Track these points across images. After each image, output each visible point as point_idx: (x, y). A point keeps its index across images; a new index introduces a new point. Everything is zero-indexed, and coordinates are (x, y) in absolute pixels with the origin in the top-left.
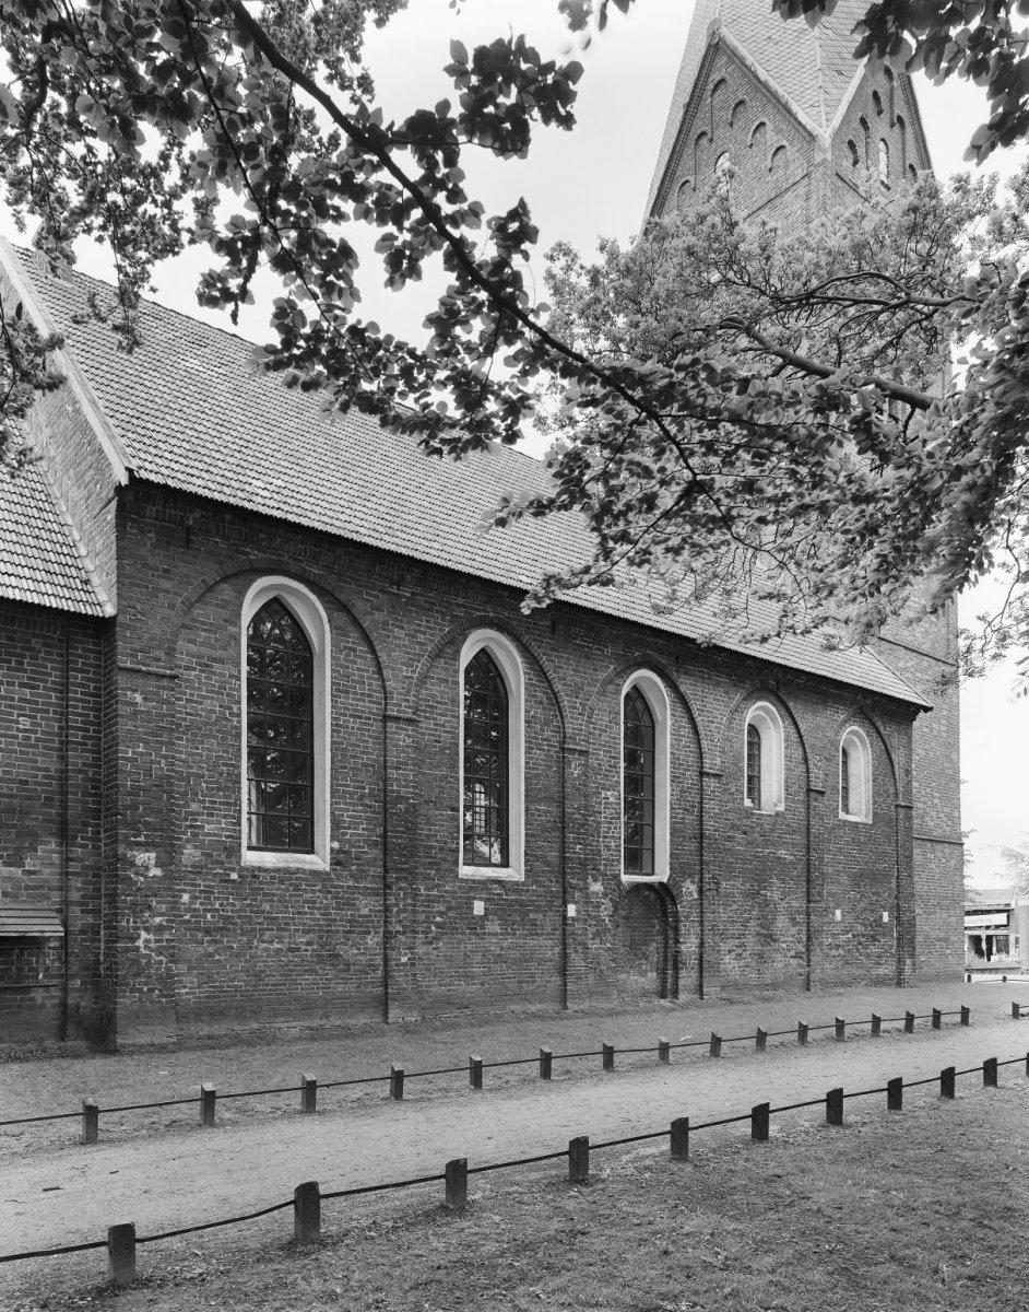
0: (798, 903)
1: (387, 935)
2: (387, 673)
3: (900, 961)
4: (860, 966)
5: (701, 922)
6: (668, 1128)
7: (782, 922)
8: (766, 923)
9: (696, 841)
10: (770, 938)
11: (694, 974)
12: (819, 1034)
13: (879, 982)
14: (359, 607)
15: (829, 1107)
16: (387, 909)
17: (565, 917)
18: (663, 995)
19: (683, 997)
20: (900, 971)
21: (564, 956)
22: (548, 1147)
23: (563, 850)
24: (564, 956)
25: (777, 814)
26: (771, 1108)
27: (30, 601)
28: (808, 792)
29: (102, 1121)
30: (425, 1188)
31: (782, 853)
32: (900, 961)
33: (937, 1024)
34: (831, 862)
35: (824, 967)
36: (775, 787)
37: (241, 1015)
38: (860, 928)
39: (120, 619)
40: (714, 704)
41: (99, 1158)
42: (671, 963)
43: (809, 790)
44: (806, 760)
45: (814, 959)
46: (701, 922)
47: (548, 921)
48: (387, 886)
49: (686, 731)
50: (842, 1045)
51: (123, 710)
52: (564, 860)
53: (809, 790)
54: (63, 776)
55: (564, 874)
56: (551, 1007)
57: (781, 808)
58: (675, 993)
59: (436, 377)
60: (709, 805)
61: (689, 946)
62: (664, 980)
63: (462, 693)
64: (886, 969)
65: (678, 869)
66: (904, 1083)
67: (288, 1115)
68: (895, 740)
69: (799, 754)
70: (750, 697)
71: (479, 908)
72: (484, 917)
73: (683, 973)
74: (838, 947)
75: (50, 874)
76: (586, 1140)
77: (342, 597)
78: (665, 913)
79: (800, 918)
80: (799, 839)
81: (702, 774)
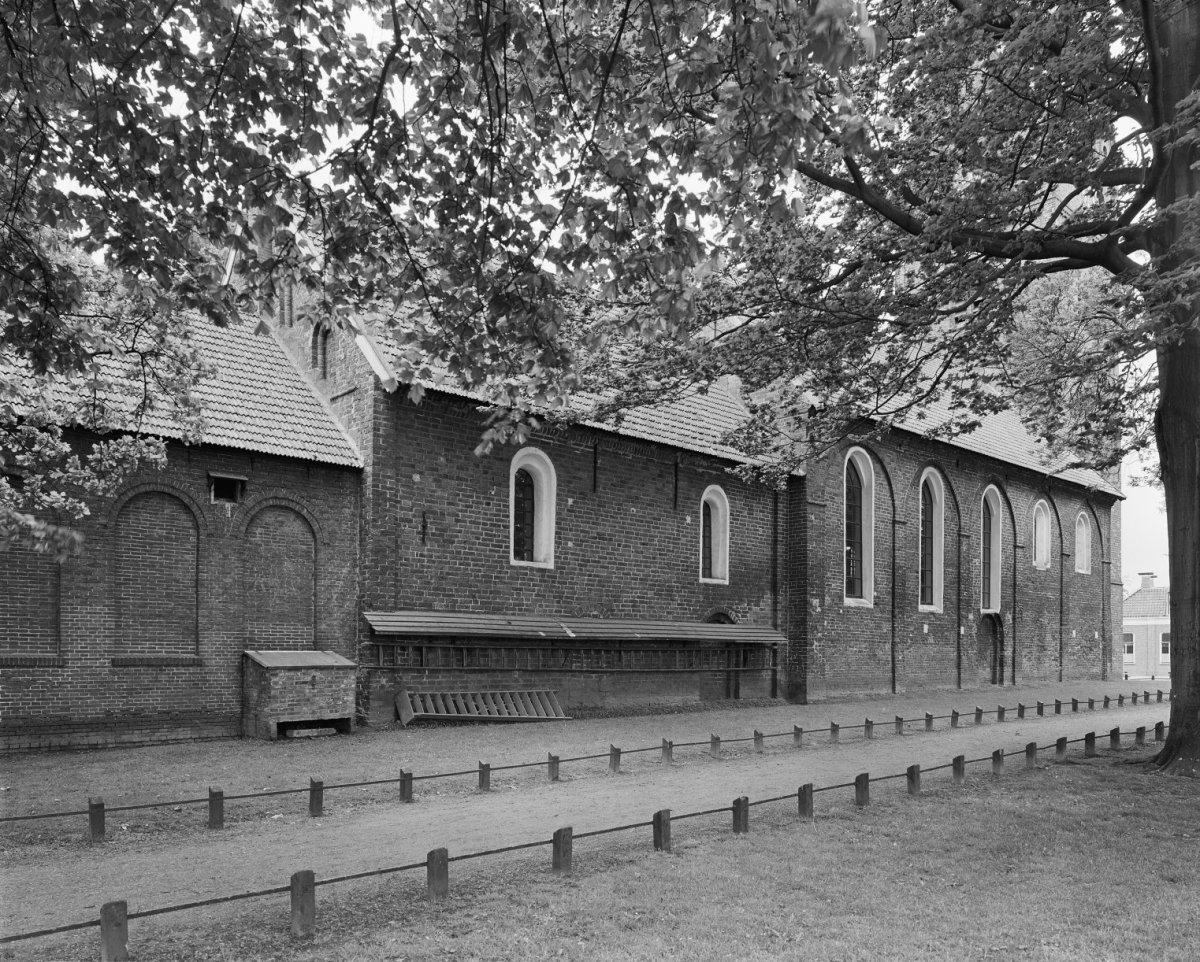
0: (1056, 626)
1: (894, 644)
2: (896, 496)
3: (1104, 664)
4: (1085, 667)
5: (1014, 638)
6: (731, 805)
7: (1049, 638)
8: (1042, 639)
9: (1012, 585)
10: (1043, 648)
11: (1010, 670)
12: (774, 741)
13: (1093, 677)
14: (886, 460)
15: (955, 768)
16: (893, 628)
17: (959, 634)
18: (994, 682)
19: (1006, 683)
20: (1104, 671)
21: (959, 657)
22: (588, 825)
23: (959, 595)
24: (959, 657)
25: (1047, 570)
26: (574, 833)
27: (1158, 496)
28: (1064, 556)
29: (984, 717)
30: (275, 899)
31: (1049, 595)
32: (1104, 664)
33: (1075, 708)
34: (1074, 603)
35: (1069, 667)
36: (1045, 553)
37: (844, 686)
38: (1084, 642)
39: (808, 476)
40: (1021, 500)
41: (489, 798)
42: (998, 663)
43: (1062, 554)
44: (1061, 535)
45: (1064, 662)
46: (1014, 638)
47: (952, 636)
48: (894, 616)
49: (1008, 521)
50: (1148, 707)
51: (809, 524)
52: (959, 600)
53: (1062, 554)
54: (774, 559)
55: (959, 609)
56: (885, 691)
57: (1049, 566)
58: (1001, 681)
59: (466, 227)
60: (1019, 565)
61: (1008, 653)
62: (994, 673)
63: (921, 506)
64: (1097, 670)
65: (1004, 606)
66: (574, 833)
67: (971, 725)
68: (1102, 520)
69: (1057, 532)
70: (1037, 498)
71: (926, 628)
72: (927, 634)
73: (1006, 669)
74: (1074, 654)
75: (768, 610)
76: (122, 905)
77: (880, 456)
78: (995, 632)
79: (1057, 636)
80: (1057, 585)
81: (1015, 547)
